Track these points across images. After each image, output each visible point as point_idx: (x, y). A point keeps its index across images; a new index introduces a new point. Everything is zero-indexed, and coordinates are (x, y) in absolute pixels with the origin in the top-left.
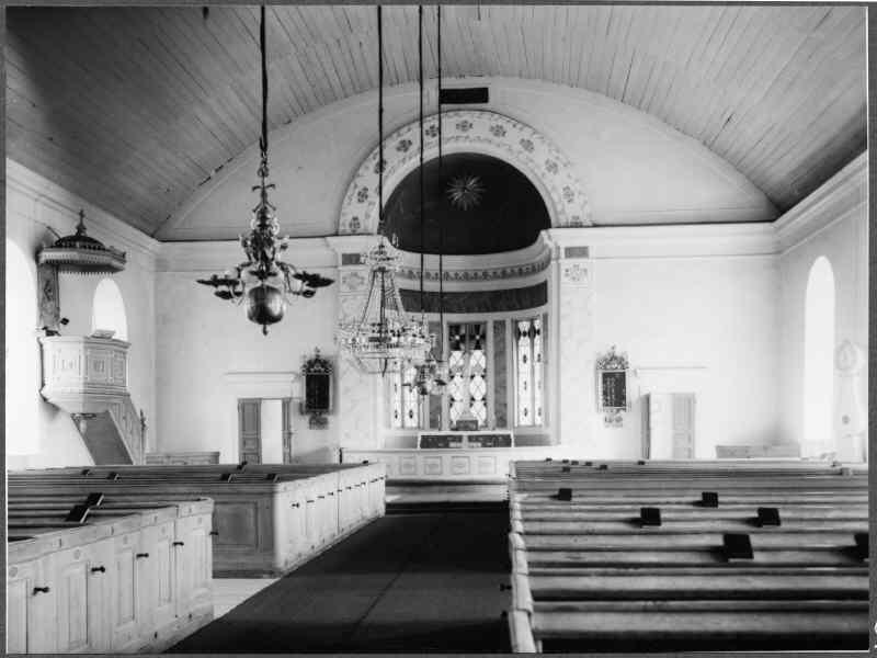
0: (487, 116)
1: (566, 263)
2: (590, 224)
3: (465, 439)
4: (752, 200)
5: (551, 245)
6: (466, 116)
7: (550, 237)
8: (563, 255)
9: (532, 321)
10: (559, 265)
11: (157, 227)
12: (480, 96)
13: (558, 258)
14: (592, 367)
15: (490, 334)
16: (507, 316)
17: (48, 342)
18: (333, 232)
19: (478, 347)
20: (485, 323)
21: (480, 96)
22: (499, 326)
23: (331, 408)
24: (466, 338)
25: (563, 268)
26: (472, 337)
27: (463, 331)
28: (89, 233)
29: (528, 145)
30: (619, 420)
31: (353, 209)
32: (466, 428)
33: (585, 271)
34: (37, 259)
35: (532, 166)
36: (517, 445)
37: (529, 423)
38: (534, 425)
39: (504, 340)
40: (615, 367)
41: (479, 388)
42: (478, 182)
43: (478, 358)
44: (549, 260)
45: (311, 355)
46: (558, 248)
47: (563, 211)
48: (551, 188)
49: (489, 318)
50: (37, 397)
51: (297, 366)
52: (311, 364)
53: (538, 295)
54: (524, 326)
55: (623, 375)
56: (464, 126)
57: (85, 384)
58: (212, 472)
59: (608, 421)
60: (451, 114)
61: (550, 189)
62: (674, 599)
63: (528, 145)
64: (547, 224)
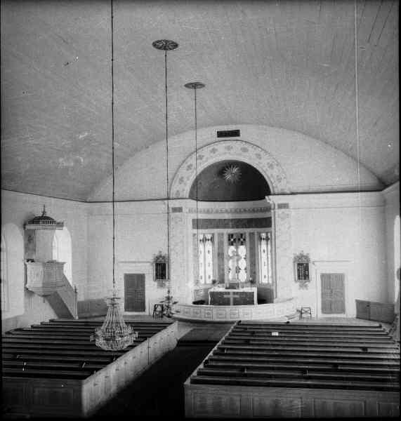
0: (239, 142)
1: (279, 212)
2: (288, 192)
3: (182, 313)
4: (371, 181)
5: (271, 202)
6: (228, 144)
7: (270, 199)
8: (276, 207)
9: (267, 233)
10: (275, 212)
11: (84, 197)
12: (236, 133)
13: (274, 209)
14: (292, 261)
15: (247, 240)
16: (255, 230)
17: (29, 265)
18: (166, 197)
19: (242, 244)
20: (245, 233)
21: (236, 133)
22: (252, 235)
23: (167, 277)
24: (235, 240)
25: (277, 214)
26: (239, 240)
27: (235, 237)
28: (48, 214)
29: (259, 156)
30: (306, 286)
31: (176, 187)
32: (234, 288)
33: (288, 215)
34: (25, 228)
35: (261, 165)
36: (234, 304)
37: (267, 282)
38: (269, 283)
39: (254, 241)
40: (304, 261)
41: (243, 264)
42: (238, 170)
43: (243, 250)
44: (103, 323)
45: (157, 254)
46: (275, 205)
47: (277, 187)
48: (270, 175)
49: (247, 231)
50: (23, 288)
51: (151, 258)
52: (158, 258)
53: (266, 223)
54: (264, 235)
55: (307, 265)
56: (229, 148)
57: (43, 284)
58: (38, 360)
59: (301, 286)
60: (222, 142)
61: (269, 175)
62: (55, 375)
63: (259, 156)
64: (269, 193)
